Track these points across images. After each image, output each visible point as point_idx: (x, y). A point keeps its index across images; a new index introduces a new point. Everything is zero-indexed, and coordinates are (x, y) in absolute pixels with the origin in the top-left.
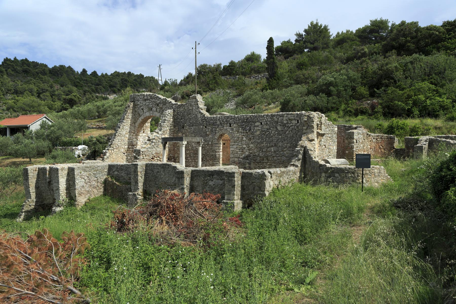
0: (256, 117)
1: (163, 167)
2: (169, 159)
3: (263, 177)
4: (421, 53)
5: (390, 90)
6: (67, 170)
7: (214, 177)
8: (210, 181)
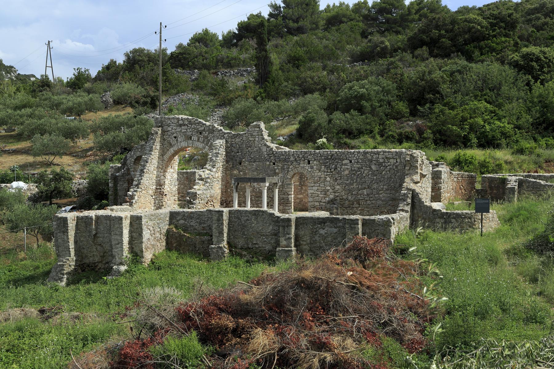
1: (255, 214)
2: (240, 205)
3: (388, 224)
4: (460, 53)
5: (438, 108)
6: (129, 219)
7: (326, 224)
8: (321, 230)
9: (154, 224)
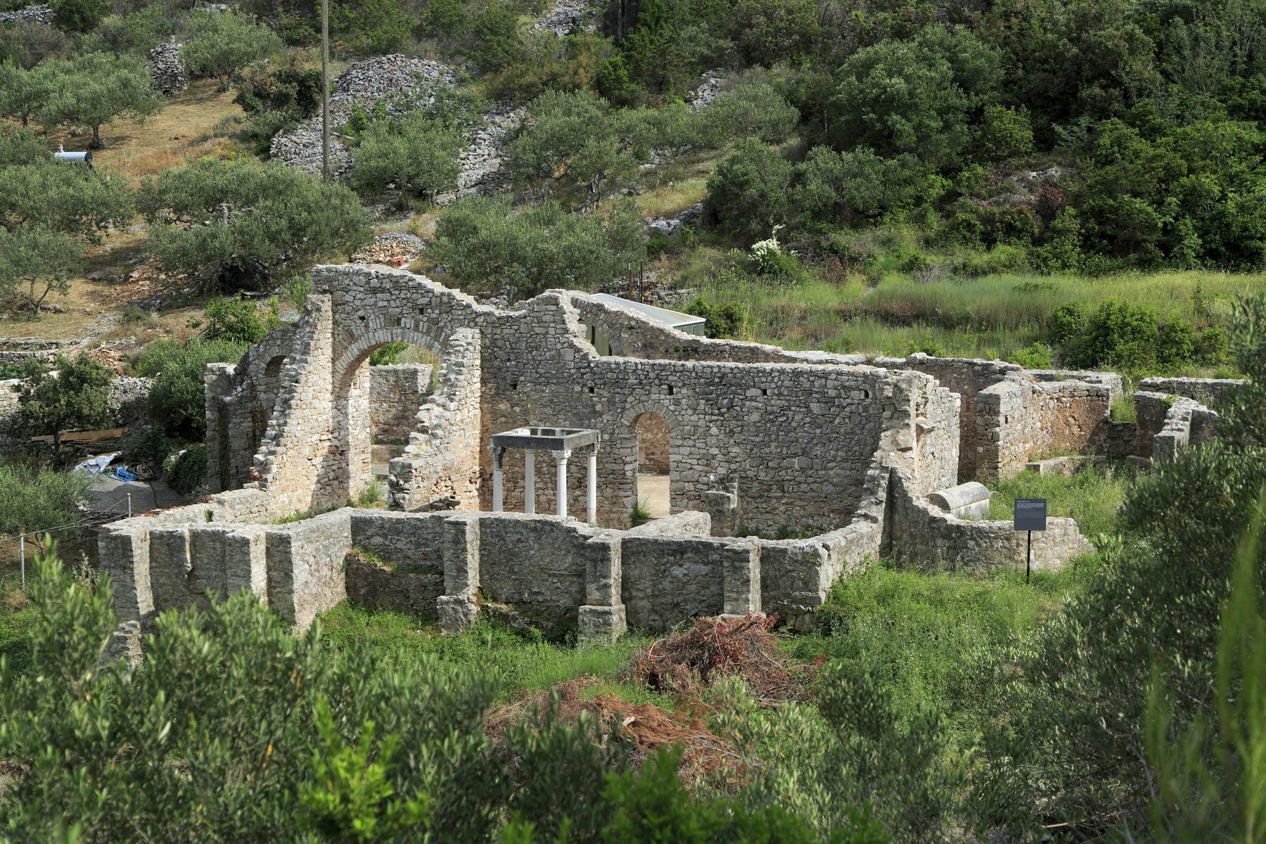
0: (749, 372)
3: (811, 561)
7: (686, 556)
8: (676, 567)
9: (317, 550)
